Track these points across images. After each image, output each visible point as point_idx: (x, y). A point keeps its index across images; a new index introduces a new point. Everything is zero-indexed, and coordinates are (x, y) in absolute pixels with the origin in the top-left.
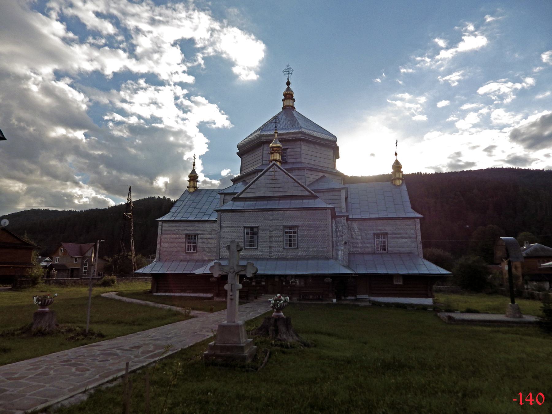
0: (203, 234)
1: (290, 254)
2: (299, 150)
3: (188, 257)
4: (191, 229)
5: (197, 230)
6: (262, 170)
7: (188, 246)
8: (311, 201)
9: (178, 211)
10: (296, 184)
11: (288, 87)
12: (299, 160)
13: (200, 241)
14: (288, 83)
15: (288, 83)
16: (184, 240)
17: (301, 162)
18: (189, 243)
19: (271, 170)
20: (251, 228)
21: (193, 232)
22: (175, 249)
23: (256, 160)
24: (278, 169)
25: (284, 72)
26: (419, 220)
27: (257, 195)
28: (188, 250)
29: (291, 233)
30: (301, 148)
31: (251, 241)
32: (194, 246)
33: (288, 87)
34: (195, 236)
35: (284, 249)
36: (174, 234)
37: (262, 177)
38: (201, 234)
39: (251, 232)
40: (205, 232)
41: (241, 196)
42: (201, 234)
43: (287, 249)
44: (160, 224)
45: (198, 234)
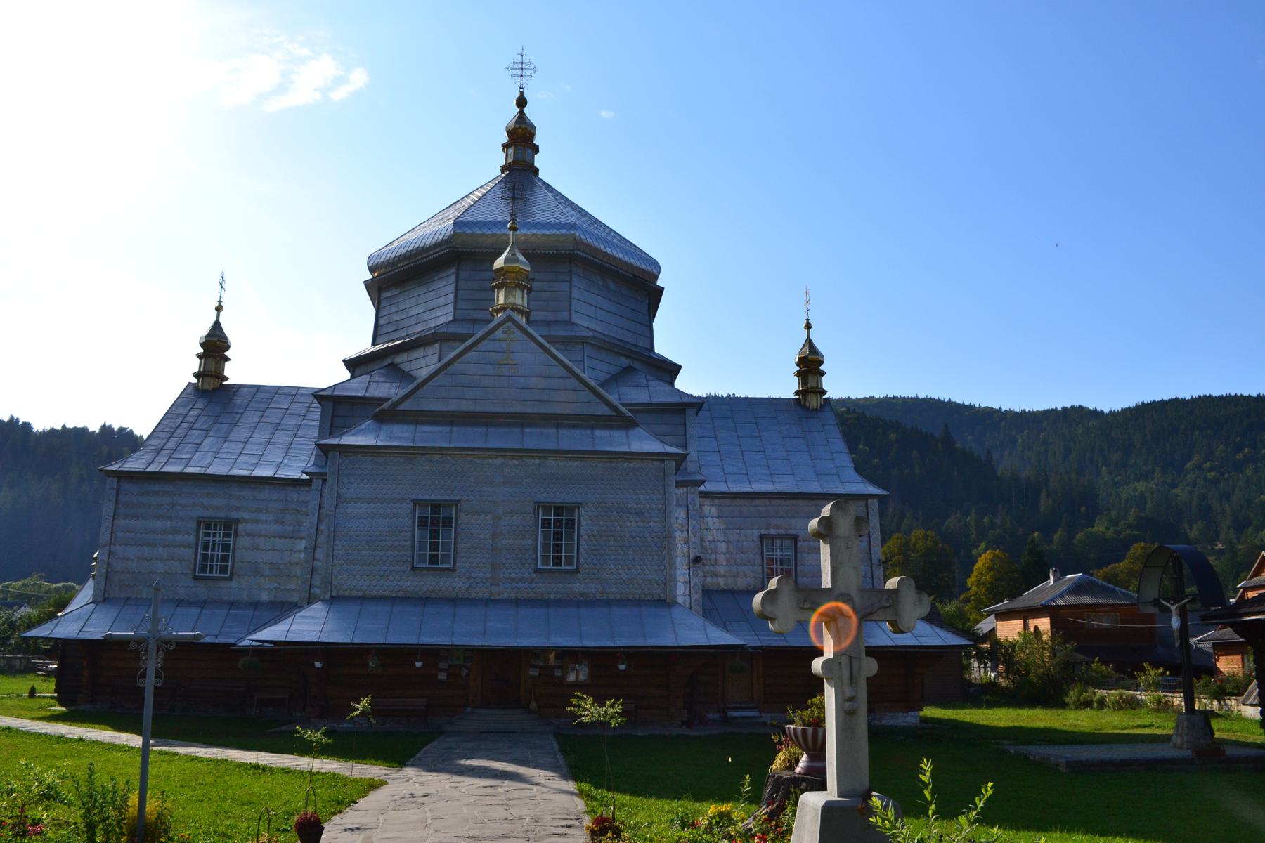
0: (257, 521)
1: (544, 587)
2: (565, 286)
3: (202, 591)
4: (215, 504)
5: (238, 509)
6: (471, 335)
7: (205, 558)
8: (618, 435)
9: (170, 445)
10: (573, 382)
11: (522, 112)
12: (564, 316)
13: (243, 541)
14: (522, 102)
15: (522, 102)
16: (192, 538)
17: (569, 323)
18: (206, 547)
19: (499, 333)
20: (436, 507)
21: (222, 514)
22: (160, 567)
23: (435, 307)
24: (518, 334)
25: (509, 69)
26: (876, 501)
27: (453, 406)
28: (203, 569)
29: (558, 524)
30: (570, 282)
31: (434, 546)
32: (224, 559)
33: (522, 112)
34: (229, 525)
35: (413, 569)
36: (157, 517)
37: (469, 355)
38: (246, 521)
39: (436, 519)
40: (263, 517)
41: (402, 407)
42: (246, 521)
43: (421, 569)
45: (237, 521)
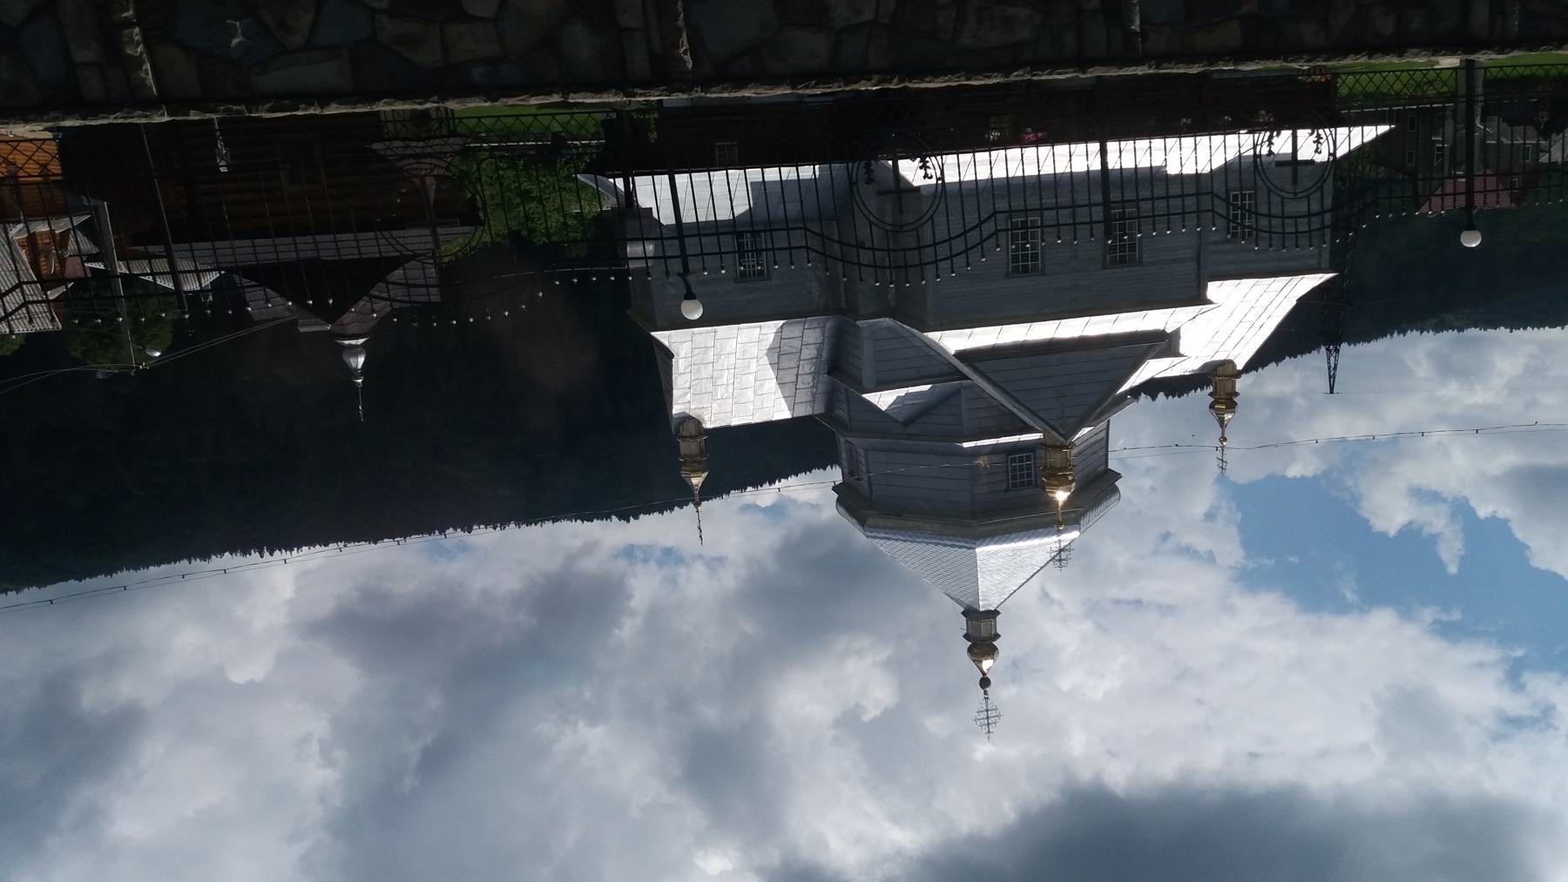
44: (1325, 264)
